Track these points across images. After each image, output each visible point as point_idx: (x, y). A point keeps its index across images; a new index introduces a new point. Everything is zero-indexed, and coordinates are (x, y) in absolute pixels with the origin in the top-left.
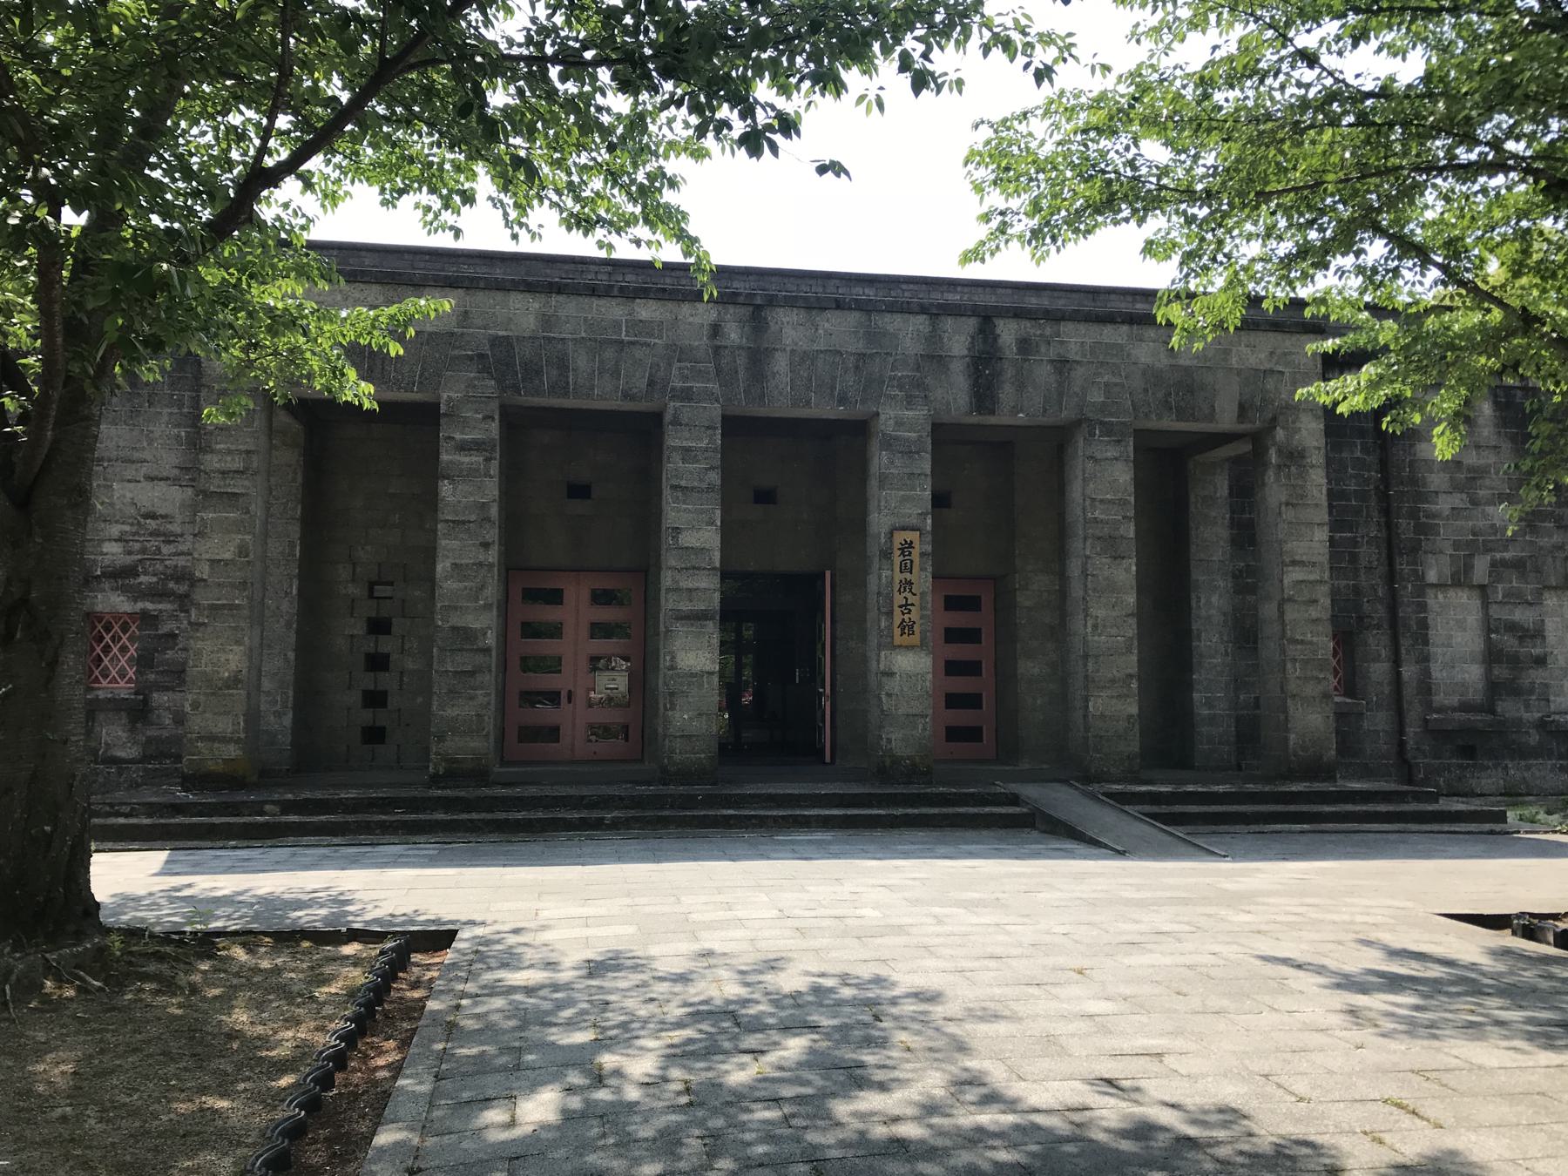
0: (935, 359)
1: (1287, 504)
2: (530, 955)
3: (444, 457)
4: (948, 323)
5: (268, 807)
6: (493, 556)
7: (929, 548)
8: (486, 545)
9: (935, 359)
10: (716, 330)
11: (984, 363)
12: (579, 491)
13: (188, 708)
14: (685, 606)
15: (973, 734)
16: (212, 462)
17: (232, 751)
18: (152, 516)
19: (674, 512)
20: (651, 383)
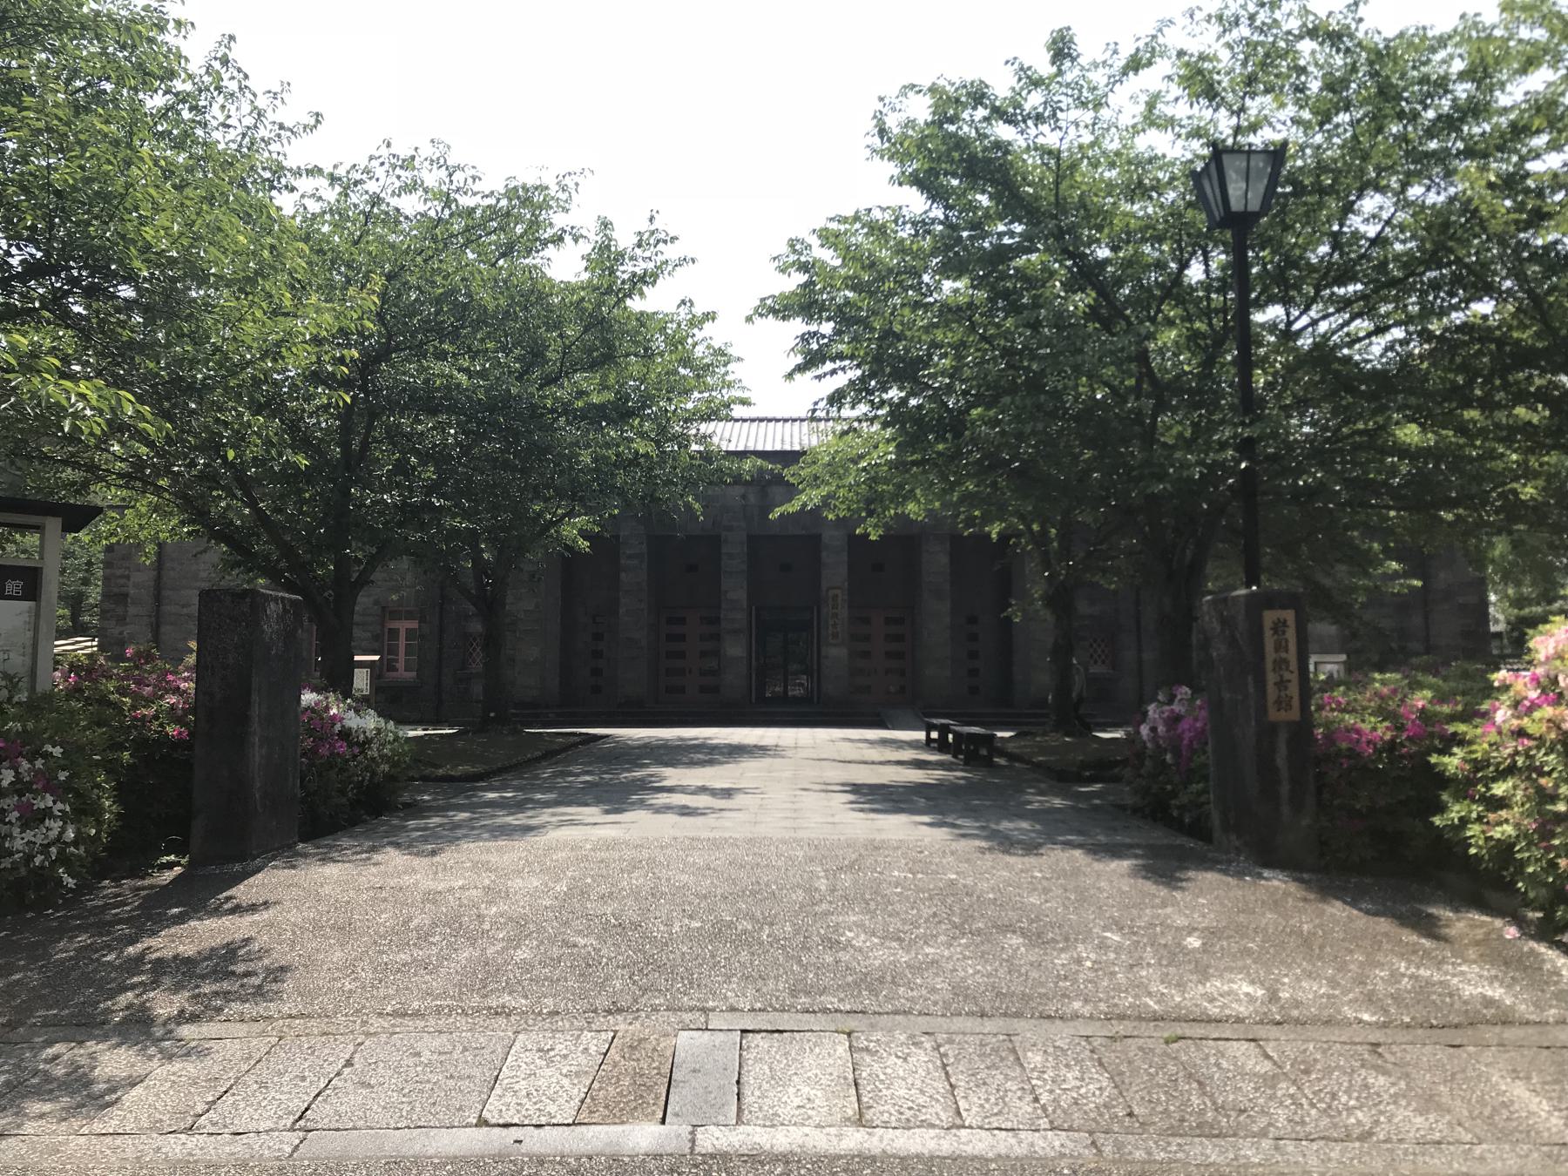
10: (744, 497)
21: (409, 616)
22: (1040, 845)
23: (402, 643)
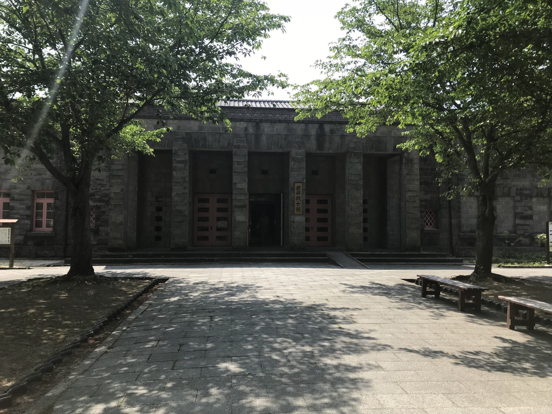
0: (306, 136)
1: (407, 174)
2: (185, 282)
3: (174, 165)
4: (310, 126)
5: (129, 256)
6: (187, 191)
7: (305, 188)
8: (185, 188)
9: (306, 136)
10: (246, 129)
11: (321, 136)
12: (213, 171)
13: (109, 231)
14: (238, 204)
15: (325, 239)
16: (114, 167)
17: (120, 242)
18: (98, 180)
19: (236, 179)
20: (229, 144)
21: (49, 196)
22: (72, 348)
23: (45, 211)
